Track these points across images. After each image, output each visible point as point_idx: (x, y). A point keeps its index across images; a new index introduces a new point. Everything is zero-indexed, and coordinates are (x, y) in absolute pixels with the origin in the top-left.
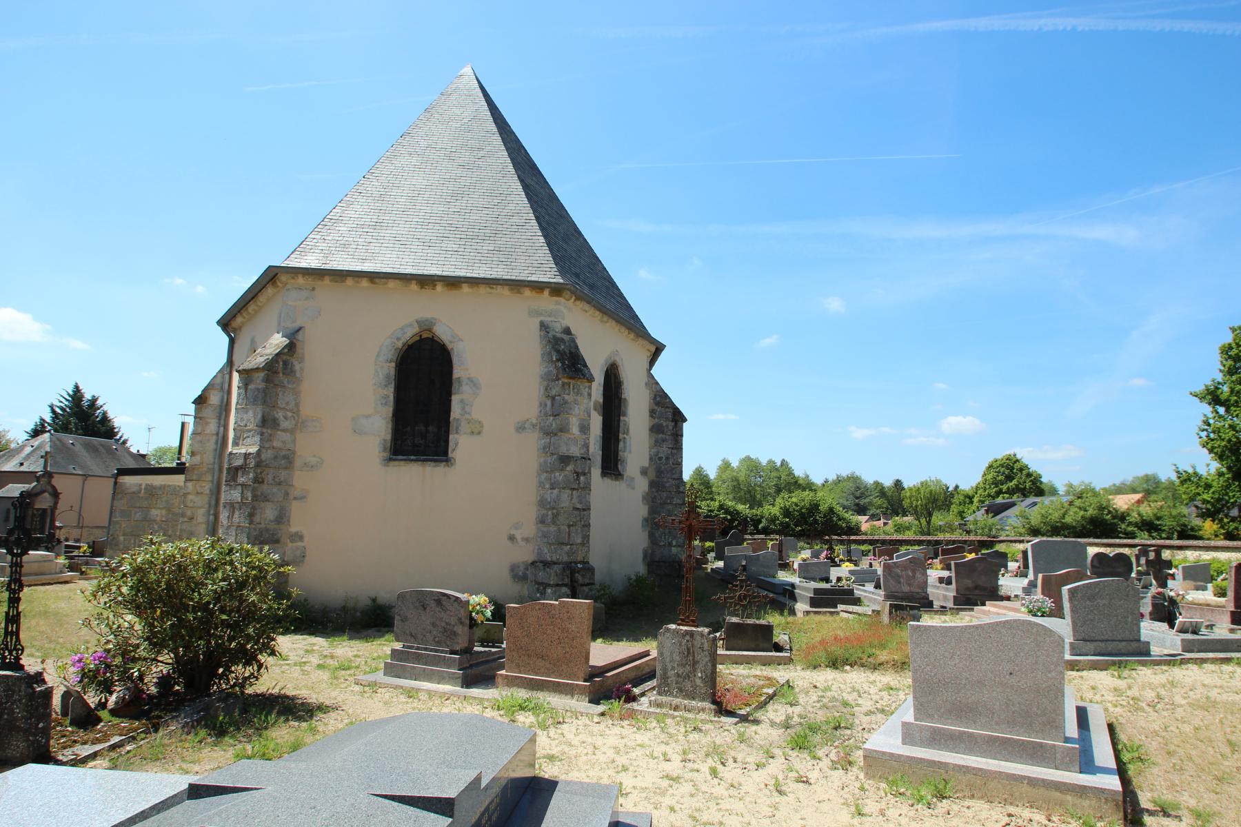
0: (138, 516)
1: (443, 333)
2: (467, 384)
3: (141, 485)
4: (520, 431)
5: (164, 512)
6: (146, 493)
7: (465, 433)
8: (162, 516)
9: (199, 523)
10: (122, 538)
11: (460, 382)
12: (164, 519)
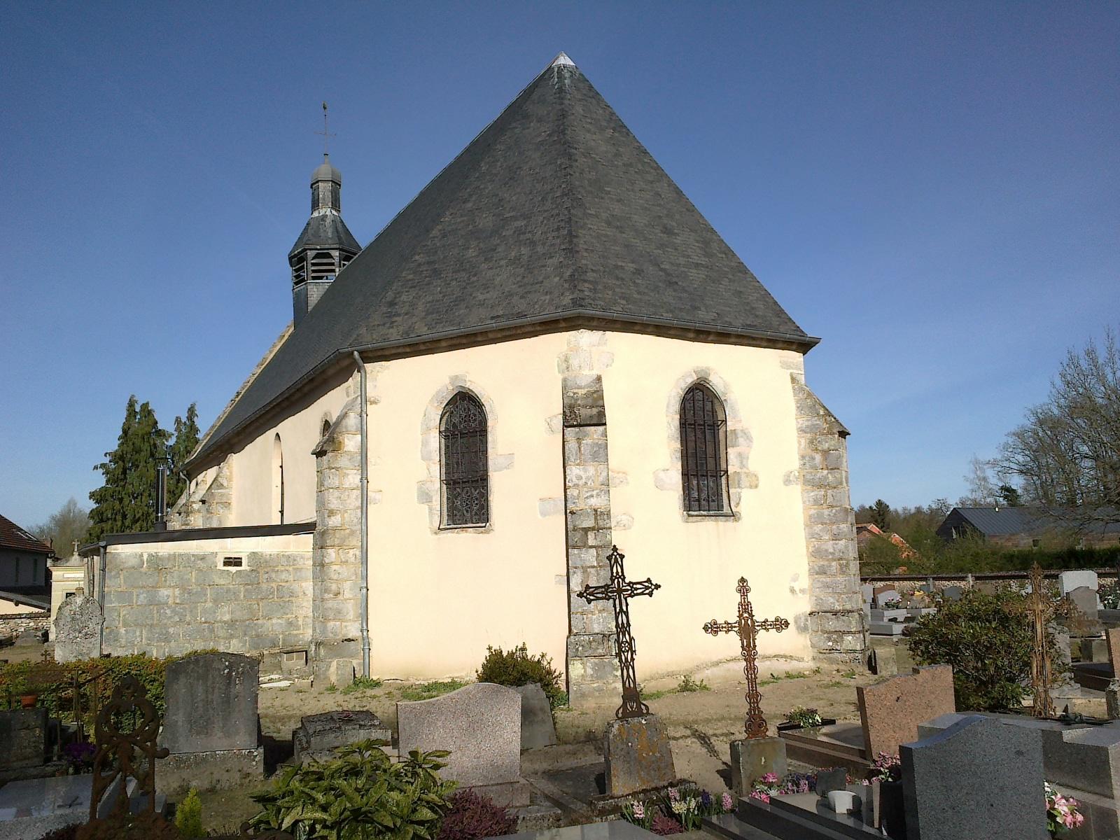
0: (143, 598)
1: (717, 383)
2: (742, 437)
3: (142, 555)
4: (787, 483)
5: (177, 591)
6: (149, 567)
7: (746, 487)
8: (175, 597)
9: (346, 600)
10: (122, 631)
11: (736, 434)
12: (178, 601)
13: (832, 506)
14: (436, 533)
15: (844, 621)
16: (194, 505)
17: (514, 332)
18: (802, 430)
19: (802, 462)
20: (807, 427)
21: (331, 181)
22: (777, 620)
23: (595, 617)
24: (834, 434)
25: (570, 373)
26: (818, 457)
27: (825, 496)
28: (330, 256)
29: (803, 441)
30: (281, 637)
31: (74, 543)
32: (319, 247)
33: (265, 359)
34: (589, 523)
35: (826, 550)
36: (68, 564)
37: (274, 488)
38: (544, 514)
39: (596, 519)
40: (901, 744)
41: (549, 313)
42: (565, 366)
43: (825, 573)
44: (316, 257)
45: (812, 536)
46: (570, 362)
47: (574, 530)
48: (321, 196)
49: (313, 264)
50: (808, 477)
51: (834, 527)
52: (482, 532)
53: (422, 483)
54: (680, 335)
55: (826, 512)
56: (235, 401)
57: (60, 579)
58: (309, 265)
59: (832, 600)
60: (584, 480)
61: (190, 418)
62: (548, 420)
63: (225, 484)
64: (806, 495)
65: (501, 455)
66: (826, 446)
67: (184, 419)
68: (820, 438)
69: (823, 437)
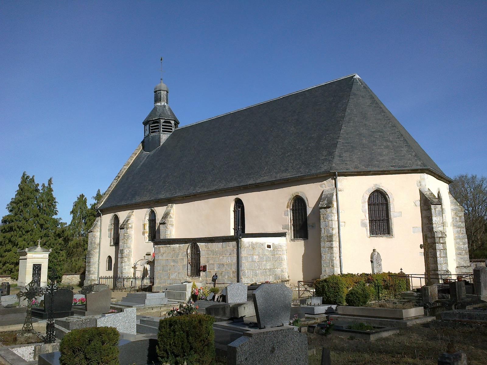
14: (370, 238)
15: (468, 269)
16: (129, 225)
17: (400, 172)
18: (452, 210)
19: (453, 220)
20: (454, 209)
21: (167, 91)
23: (443, 265)
24: (463, 211)
25: (422, 187)
26: (458, 218)
29: (453, 213)
30: (280, 275)
31: (38, 240)
32: (166, 119)
33: (129, 163)
34: (440, 236)
35: (461, 248)
36: (35, 251)
38: (414, 232)
39: (442, 234)
40: (250, 339)
41: (414, 167)
42: (419, 184)
43: (461, 255)
45: (456, 243)
47: (437, 237)
48: (162, 97)
49: (163, 125)
51: (464, 240)
53: (362, 220)
54: (383, 173)
55: (461, 235)
56: (118, 180)
57: (31, 257)
58: (161, 125)
60: (437, 222)
61: (49, 185)
63: (172, 217)
64: (454, 230)
65: (396, 212)
66: (460, 215)
67: (46, 185)
68: (458, 212)
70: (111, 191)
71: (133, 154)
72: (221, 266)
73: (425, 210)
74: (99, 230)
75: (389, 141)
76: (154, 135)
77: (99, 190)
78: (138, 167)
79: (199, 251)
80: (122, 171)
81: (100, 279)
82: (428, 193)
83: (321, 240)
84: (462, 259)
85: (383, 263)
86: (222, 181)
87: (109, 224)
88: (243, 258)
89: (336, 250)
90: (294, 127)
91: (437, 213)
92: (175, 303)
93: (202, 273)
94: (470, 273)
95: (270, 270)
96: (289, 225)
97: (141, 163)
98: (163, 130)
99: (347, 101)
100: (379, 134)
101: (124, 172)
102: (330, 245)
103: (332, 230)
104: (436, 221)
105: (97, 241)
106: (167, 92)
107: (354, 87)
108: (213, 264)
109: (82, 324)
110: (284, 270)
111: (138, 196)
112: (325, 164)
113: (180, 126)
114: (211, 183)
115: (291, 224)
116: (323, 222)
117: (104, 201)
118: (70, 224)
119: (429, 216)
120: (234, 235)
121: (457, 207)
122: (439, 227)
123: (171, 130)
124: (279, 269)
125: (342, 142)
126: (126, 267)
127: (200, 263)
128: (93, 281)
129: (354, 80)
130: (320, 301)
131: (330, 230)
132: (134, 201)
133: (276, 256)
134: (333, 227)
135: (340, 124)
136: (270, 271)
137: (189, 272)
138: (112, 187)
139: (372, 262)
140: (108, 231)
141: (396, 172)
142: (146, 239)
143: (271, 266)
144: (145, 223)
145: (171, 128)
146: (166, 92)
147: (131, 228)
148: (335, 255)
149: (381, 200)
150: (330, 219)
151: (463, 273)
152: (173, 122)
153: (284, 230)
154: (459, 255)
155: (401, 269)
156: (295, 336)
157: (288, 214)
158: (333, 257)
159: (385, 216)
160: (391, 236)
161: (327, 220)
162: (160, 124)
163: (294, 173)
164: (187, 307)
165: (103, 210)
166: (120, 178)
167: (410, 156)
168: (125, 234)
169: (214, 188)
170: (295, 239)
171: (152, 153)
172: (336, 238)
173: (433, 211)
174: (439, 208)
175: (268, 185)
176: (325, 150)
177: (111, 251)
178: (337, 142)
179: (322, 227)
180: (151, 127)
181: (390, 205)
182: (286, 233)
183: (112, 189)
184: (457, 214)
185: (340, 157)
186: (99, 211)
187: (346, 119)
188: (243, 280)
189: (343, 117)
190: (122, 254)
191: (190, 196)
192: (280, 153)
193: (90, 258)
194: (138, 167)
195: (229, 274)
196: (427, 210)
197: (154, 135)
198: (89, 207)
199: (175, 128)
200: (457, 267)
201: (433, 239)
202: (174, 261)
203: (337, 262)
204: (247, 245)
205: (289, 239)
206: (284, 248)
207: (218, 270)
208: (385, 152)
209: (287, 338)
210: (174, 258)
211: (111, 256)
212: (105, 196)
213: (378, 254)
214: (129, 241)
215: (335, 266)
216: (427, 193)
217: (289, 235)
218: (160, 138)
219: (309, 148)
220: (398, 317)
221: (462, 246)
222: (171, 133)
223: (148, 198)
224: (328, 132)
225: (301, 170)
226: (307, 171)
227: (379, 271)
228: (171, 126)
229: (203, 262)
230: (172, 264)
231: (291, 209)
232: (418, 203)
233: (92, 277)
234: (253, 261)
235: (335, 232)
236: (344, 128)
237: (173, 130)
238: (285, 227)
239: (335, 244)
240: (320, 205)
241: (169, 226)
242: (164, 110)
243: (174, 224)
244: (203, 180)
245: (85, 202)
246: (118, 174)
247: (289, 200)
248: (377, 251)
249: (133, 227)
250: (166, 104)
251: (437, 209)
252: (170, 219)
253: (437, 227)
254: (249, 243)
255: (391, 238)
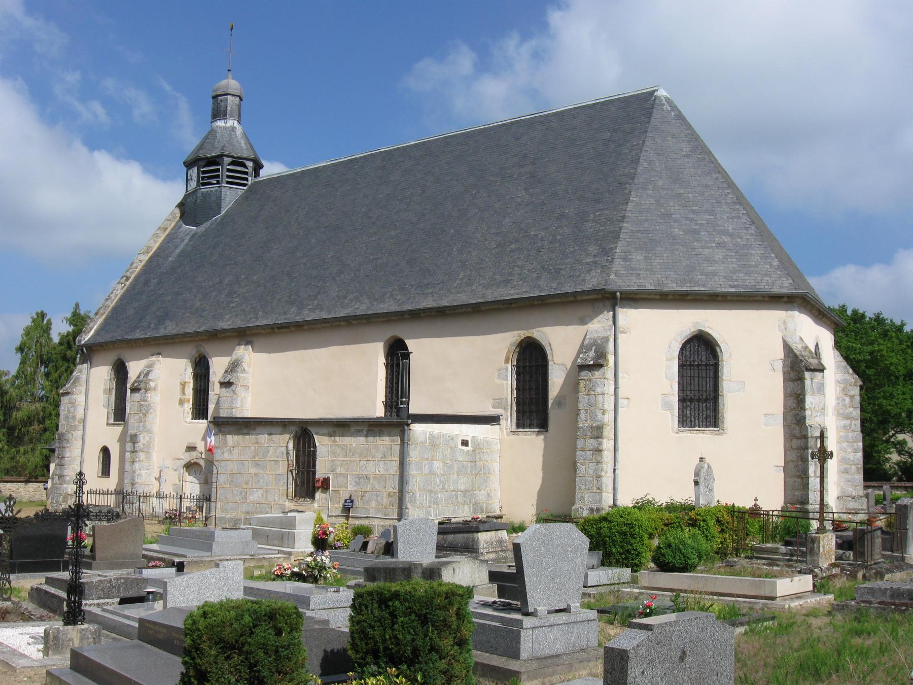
13: (854, 431)
14: (677, 433)
16: (151, 383)
18: (838, 382)
20: (842, 380)
22: (109, 512)
26: (847, 399)
27: (850, 424)
28: (245, 166)
29: (838, 388)
37: (379, 380)
43: (847, 473)
44: (231, 164)
46: (788, 325)
49: (229, 170)
50: (841, 411)
51: (855, 444)
52: (716, 434)
53: (665, 395)
55: (850, 435)
56: (125, 284)
58: (225, 170)
59: (851, 489)
60: (814, 405)
62: (772, 362)
63: (246, 369)
69: (851, 387)
70: (110, 308)
71: (160, 228)
72: (362, 480)
73: (791, 381)
74: (84, 391)
75: (725, 232)
76: (208, 190)
77: (77, 305)
78: (170, 259)
79: (315, 446)
80: (134, 265)
81: (88, 493)
82: (800, 346)
83: (578, 434)
84: (849, 481)
85: (716, 486)
86: (361, 299)
87: (106, 378)
88: (413, 466)
89: (607, 456)
90: (525, 189)
91: (815, 388)
92: (272, 552)
93: (318, 495)
94: (862, 510)
95: (465, 492)
96: (507, 399)
97: (178, 251)
98: (228, 180)
99: (641, 142)
100: (707, 217)
101: (139, 268)
102: (596, 445)
103: (604, 414)
104: (812, 404)
105: (80, 413)
106: (241, 99)
107: (656, 115)
108: (344, 476)
109: (109, 588)
110: (493, 495)
111: (172, 320)
112: (593, 273)
113: (264, 173)
114: (336, 302)
115: (513, 399)
116: (585, 396)
117: (95, 328)
118: (15, 375)
119: (799, 392)
120: (385, 415)
121: (847, 377)
122: (817, 416)
123: (246, 182)
124: (482, 492)
125: (631, 228)
126: (143, 472)
127: (314, 473)
128: (69, 497)
129: (655, 99)
130: (596, 560)
131: (598, 414)
132: (162, 332)
133: (478, 464)
134: (606, 407)
135: (627, 191)
136: (465, 494)
137: (290, 490)
138: (114, 300)
139: (696, 483)
140: (104, 394)
141: (739, 299)
142: (186, 415)
143: (467, 484)
144: (186, 380)
145: (247, 176)
146: (238, 99)
147: (155, 389)
148: (605, 467)
149: (704, 357)
150: (599, 390)
151: (848, 509)
152: (250, 164)
153: (496, 410)
154: (845, 473)
155: (756, 500)
156: (717, 629)
157: (507, 376)
158: (602, 470)
159: (712, 390)
160: (721, 431)
161: (594, 393)
162: (222, 168)
163: (524, 290)
164: (313, 563)
165: (94, 348)
166: (130, 281)
167: (768, 266)
168: (142, 403)
169: (343, 313)
170: (519, 430)
171: (202, 228)
172: (608, 432)
173: (808, 382)
174: (819, 378)
175: (465, 312)
176: (594, 242)
177: (110, 436)
178: (621, 228)
179: (580, 406)
180: (203, 174)
181: (723, 367)
182: (501, 417)
183: (114, 303)
184: (846, 390)
185: (625, 259)
186: (84, 349)
187: (639, 180)
188: (410, 512)
189: (633, 177)
190: (134, 443)
191: (288, 327)
192: (494, 245)
193: (64, 448)
194: (170, 259)
195: (379, 499)
196: (795, 380)
197: (208, 190)
198: (56, 339)
199: (255, 177)
200: (838, 498)
201: (803, 440)
202: (257, 465)
203: (607, 480)
204: (421, 439)
205: (506, 429)
206: (497, 447)
207: (355, 488)
208: (717, 256)
209: (704, 633)
210: (257, 459)
211: (108, 447)
212: (97, 317)
213: (709, 466)
214: (150, 418)
215: (604, 489)
216: (797, 347)
217: (506, 420)
218: (219, 198)
219: (558, 237)
220: (768, 594)
221: (851, 456)
222: (245, 188)
223: (193, 327)
224: (600, 206)
225: (541, 283)
226: (554, 285)
227: (709, 503)
228: (246, 173)
229: (321, 471)
230: (253, 470)
231: (514, 366)
232: (779, 366)
233: (66, 488)
234: (432, 473)
235: (608, 418)
236: (635, 199)
237: (249, 183)
238: (499, 403)
239: (607, 444)
240: (579, 360)
241: (239, 390)
242: (233, 136)
243: (250, 385)
244: (319, 293)
245: (47, 329)
246: (126, 272)
247: (511, 345)
248: (707, 460)
249: (159, 387)
250: (236, 124)
251: (815, 380)
252: (242, 375)
253: (813, 419)
254: (426, 434)
255: (720, 434)
